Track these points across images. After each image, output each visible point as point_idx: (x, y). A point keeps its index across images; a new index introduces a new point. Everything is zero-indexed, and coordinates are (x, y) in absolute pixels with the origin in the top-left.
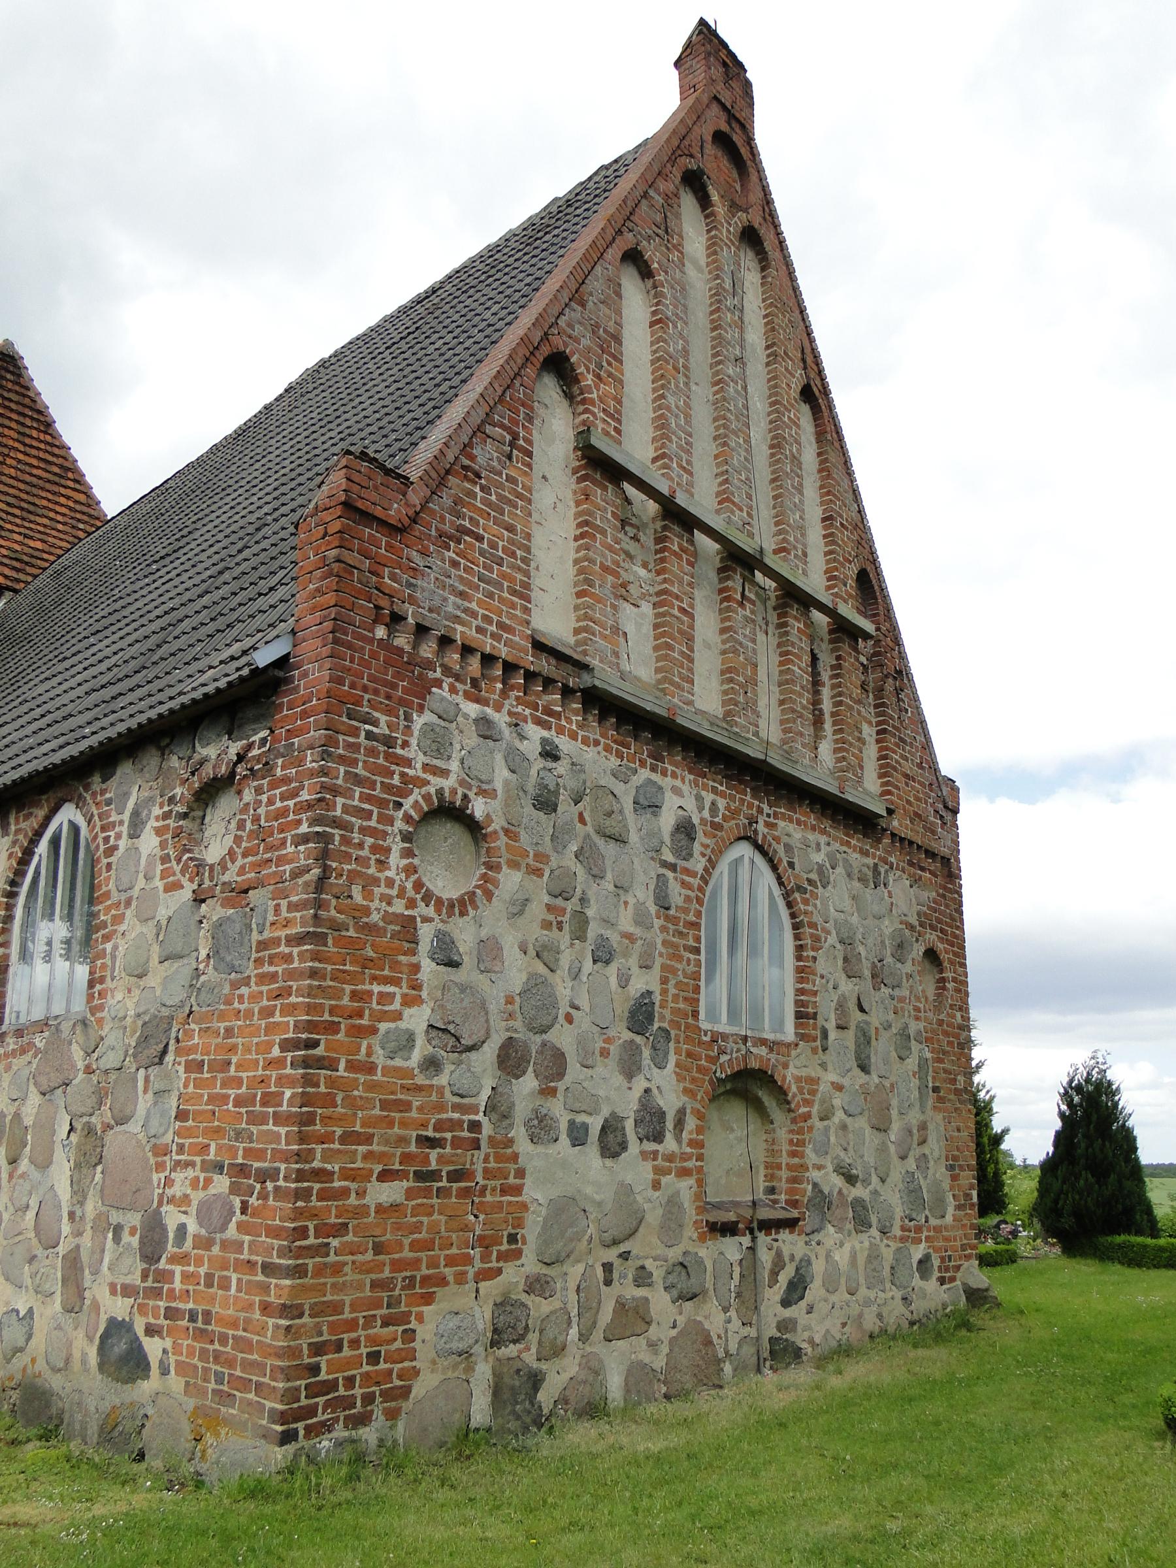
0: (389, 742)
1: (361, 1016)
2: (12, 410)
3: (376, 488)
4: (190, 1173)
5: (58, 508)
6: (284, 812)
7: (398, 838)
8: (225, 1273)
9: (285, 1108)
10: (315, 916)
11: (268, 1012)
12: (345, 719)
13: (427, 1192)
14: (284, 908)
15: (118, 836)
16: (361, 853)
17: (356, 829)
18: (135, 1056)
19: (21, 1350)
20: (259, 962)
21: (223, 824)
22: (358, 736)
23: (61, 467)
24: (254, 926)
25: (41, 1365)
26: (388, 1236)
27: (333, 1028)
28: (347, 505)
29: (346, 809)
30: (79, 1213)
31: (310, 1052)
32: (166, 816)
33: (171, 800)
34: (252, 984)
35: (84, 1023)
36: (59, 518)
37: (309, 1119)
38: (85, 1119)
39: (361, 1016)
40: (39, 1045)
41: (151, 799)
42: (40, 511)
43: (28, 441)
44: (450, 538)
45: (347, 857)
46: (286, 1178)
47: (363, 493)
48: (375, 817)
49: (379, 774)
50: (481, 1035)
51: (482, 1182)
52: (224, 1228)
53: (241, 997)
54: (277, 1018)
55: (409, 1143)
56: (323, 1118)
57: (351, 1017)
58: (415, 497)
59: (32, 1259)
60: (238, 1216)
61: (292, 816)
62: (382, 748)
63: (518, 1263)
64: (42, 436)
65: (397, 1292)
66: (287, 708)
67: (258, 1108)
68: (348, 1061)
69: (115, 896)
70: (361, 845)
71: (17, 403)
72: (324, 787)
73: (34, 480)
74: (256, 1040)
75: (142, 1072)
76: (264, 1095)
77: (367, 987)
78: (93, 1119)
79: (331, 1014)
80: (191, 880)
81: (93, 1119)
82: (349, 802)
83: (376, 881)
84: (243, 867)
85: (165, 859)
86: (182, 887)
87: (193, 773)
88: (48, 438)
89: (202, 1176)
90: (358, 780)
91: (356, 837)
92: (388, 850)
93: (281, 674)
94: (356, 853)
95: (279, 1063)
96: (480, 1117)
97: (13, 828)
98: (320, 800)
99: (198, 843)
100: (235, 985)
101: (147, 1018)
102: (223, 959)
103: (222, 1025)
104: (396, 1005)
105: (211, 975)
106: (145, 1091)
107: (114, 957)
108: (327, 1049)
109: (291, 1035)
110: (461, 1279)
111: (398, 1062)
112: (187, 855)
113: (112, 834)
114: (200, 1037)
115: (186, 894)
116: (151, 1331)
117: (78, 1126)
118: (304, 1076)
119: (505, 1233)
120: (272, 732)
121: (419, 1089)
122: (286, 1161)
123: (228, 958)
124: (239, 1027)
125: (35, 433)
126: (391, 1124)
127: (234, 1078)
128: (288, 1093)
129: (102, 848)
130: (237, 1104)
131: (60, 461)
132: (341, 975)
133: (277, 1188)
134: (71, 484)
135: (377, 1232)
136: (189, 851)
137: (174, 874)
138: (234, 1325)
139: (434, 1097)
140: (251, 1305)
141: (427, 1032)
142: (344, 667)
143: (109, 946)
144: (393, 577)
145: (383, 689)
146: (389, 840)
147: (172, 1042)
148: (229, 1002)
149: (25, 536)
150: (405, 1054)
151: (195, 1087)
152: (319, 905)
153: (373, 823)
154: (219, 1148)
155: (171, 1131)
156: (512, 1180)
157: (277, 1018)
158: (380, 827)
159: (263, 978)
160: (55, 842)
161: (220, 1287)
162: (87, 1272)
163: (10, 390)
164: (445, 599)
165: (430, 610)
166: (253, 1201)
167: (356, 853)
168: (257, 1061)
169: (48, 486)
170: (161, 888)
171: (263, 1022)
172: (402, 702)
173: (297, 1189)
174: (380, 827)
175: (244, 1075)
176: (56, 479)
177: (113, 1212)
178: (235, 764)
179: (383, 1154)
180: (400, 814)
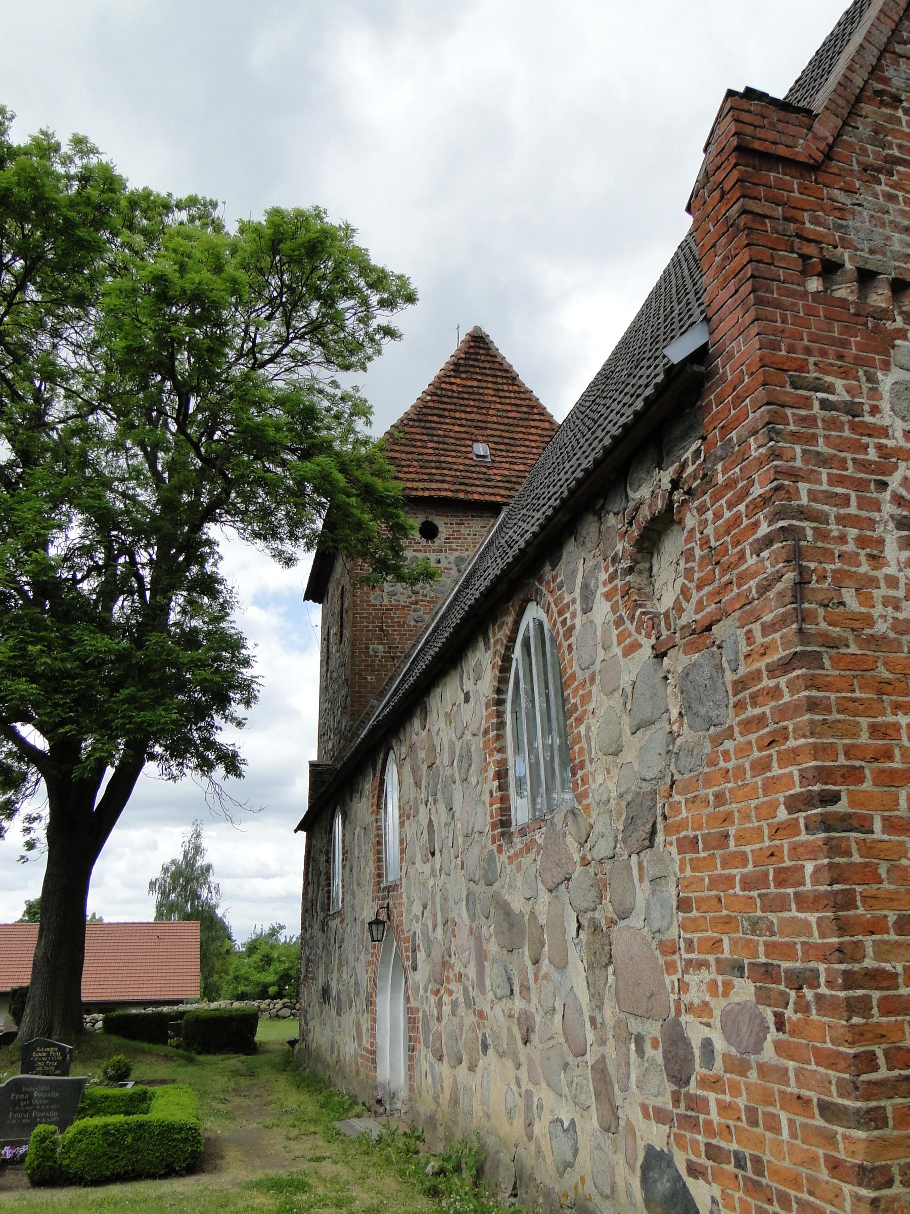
0: (853, 410)
1: (890, 757)
2: (487, 375)
3: (773, 126)
4: (706, 975)
5: (531, 437)
6: (736, 520)
7: (891, 526)
8: (770, 1109)
9: (809, 886)
10: (800, 630)
11: (762, 766)
12: (789, 389)
14: (757, 633)
15: (574, 616)
16: (844, 548)
17: (832, 519)
18: (624, 841)
19: (570, 1165)
20: (739, 706)
21: (672, 568)
22: (810, 407)
23: (528, 406)
24: (725, 665)
25: (589, 1188)
27: (853, 775)
28: (742, 150)
29: (813, 496)
30: (599, 1020)
31: (830, 809)
32: (612, 578)
33: (614, 560)
34: (737, 735)
35: (573, 812)
36: (533, 444)
37: (846, 901)
38: (589, 915)
39: (890, 757)
40: (540, 841)
41: (596, 567)
42: (518, 443)
43: (502, 394)
44: (879, 170)
45: (827, 554)
46: (830, 984)
47: (760, 133)
48: (853, 501)
49: (848, 450)
52: (758, 1048)
53: (726, 753)
54: (776, 771)
56: (864, 898)
57: (876, 760)
58: (825, 129)
59: (566, 1065)
60: (773, 1034)
61: (745, 522)
62: (845, 418)
64: (511, 388)
66: (716, 406)
67: (773, 889)
68: (884, 819)
69: (580, 676)
70: (843, 539)
71: (490, 369)
72: (778, 471)
73: (511, 421)
74: (754, 803)
75: (634, 857)
76: (778, 872)
77: (891, 719)
78: (597, 915)
79: (847, 755)
80: (648, 636)
81: (597, 915)
82: (816, 487)
83: (873, 582)
84: (700, 602)
85: (619, 622)
86: (640, 646)
87: (630, 524)
88: (515, 388)
89: (720, 979)
90: (825, 461)
91: (834, 529)
92: (881, 542)
93: (702, 369)
94: (837, 549)
95: (790, 828)
97: (492, 641)
98: (776, 489)
99: (650, 597)
100: (717, 741)
101: (629, 797)
102: (697, 714)
103: (710, 792)
105: (687, 735)
106: (641, 880)
107: (588, 739)
108: (852, 803)
109: (798, 790)
112: (640, 610)
113: (568, 615)
114: (688, 810)
115: (646, 652)
116: (694, 1171)
117: (585, 923)
118: (827, 842)
120: (704, 438)
122: (825, 959)
123: (703, 712)
124: (731, 791)
125: (506, 388)
127: (734, 855)
128: (809, 867)
129: (561, 632)
130: (747, 884)
131: (527, 402)
132: (851, 705)
133: (819, 998)
134: (537, 417)
136: (641, 606)
137: (630, 635)
138: (795, 1183)
140: (814, 1159)
142: (776, 329)
143: (582, 729)
144: (815, 221)
145: (831, 350)
146: (879, 529)
147: (659, 820)
148: (713, 763)
149: (511, 463)
151: (693, 869)
152: (803, 617)
153: (853, 510)
154: (734, 943)
155: (675, 924)
157: (776, 771)
158: (863, 514)
159: (748, 725)
160: (526, 644)
161: (768, 1128)
162: (616, 1088)
163: (483, 361)
164: (888, 238)
165: (872, 252)
166: (789, 1013)
167: (837, 549)
168: (760, 829)
169: (521, 423)
170: (620, 654)
171: (759, 780)
172: (859, 361)
173: (847, 999)
174: (863, 514)
175: (747, 849)
176: (526, 416)
177: (632, 1020)
178: (671, 493)
180: (887, 495)
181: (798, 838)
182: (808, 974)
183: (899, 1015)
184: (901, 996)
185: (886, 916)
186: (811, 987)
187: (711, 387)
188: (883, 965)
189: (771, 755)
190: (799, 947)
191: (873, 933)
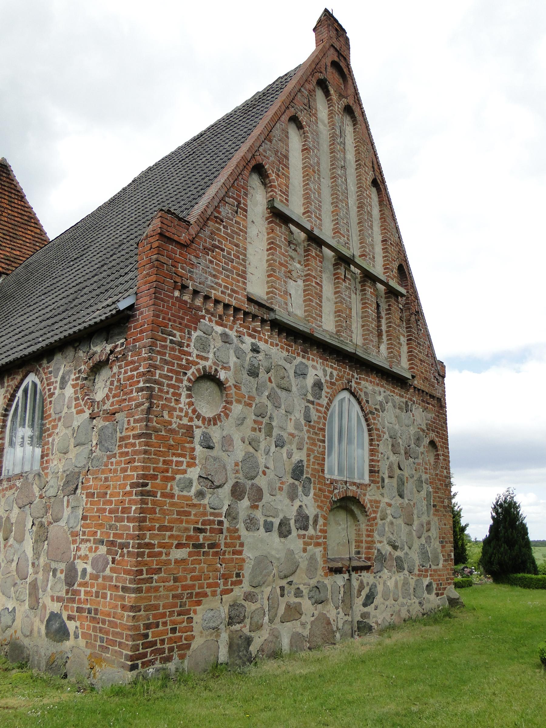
0: (181, 344)
1: (168, 472)
2: (6, 191)
3: (174, 226)
4: (88, 545)
5: (27, 236)
6: (132, 377)
7: (185, 389)
8: (105, 591)
9: (132, 514)
10: (146, 425)
11: (124, 470)
12: (160, 334)
13: (198, 554)
14: (132, 422)
15: (55, 388)
16: (167, 396)
17: (165, 385)
18: (63, 490)
19: (10, 627)
20: (120, 447)
21: (104, 383)
22: (166, 342)
23: (28, 217)
24: (118, 430)
25: (19, 634)
26: (180, 574)
27: (154, 477)
28: (161, 234)
29: (161, 376)
30: (36, 563)
31: (144, 488)
32: (77, 379)
33: (80, 371)
34: (117, 457)
35: (39, 475)
36: (28, 241)
37: (144, 520)
38: (40, 520)
39: (168, 472)
40: (18, 485)
41: (70, 371)
42: (18, 237)
43: (13, 205)
44: (209, 250)
45: (161, 398)
46: (133, 547)
47: (169, 229)
48: (174, 379)
49: (176, 359)
50: (223, 480)
51: (224, 549)
52: (104, 570)
53: (112, 463)
54: (129, 473)
55: (190, 531)
56: (150, 519)
57: (163, 472)
58: (193, 231)
59: (15, 585)
60: (110, 565)
61: (135, 379)
62: (177, 347)
63: (241, 586)
64: (19, 203)
65: (184, 600)
66: (133, 329)
67: (120, 514)
68: (161, 493)
69: (53, 416)
70: (167, 393)
71: (8, 187)
72: (150, 365)
73: (16, 223)
74: (119, 483)
75: (66, 498)
76: (123, 508)
77: (170, 458)
78: (43, 520)
79: (154, 471)
80: (89, 409)
81: (43, 520)
82: (162, 372)
83: (175, 409)
84: (113, 403)
85: (77, 399)
86: (85, 412)
87: (89, 359)
88: (22, 203)
89: (94, 546)
90: (166, 362)
91: (165, 388)
92: (180, 395)
93: (131, 313)
94: (165, 396)
95: (129, 493)
96: (223, 519)
97: (6, 384)
98: (148, 371)
99: (92, 391)
100: (109, 457)
101: (68, 473)
102: (103, 445)
103: (103, 476)
104: (184, 467)
105: (98, 453)
106: (67, 507)
107: (53, 445)
108: (152, 487)
109: (135, 481)
110: (214, 594)
111: (185, 493)
112: (87, 397)
113: (52, 387)
114: (93, 482)
115: (86, 415)
116: (70, 618)
117: (36, 523)
118: (141, 500)
119: (235, 573)
120: (126, 340)
121: (194, 505)
122: (133, 539)
123: (106, 445)
124: (111, 477)
125: (16, 201)
126: (181, 522)
127: (109, 501)
128: (134, 508)
129: (47, 394)
130: (110, 512)
131: (28, 214)
132: (158, 453)
133: (128, 552)
134: (33, 225)
135: (175, 572)
136: (88, 395)
137: (81, 406)
138: (109, 615)
139: (201, 510)
140: (117, 606)
141: (198, 479)
142: (160, 309)
143: (50, 439)
144: (182, 268)
145: (178, 320)
146: (181, 390)
147: (80, 484)
148: (106, 465)
149: (12, 249)
150: (188, 489)
151: (91, 505)
152: (148, 420)
153: (173, 382)
154: (102, 533)
155: (79, 525)
156: (238, 548)
157: (129, 473)
158: (177, 384)
159: (122, 454)
160: (26, 391)
161: (102, 598)
162: (40, 590)
163: (4, 181)
164: (207, 278)
165: (200, 283)
166: (117, 557)
167: (165, 396)
168: (119, 493)
169: (22, 226)
170: (75, 413)
171: (122, 475)
172: (187, 326)
173: (138, 552)
174: (177, 384)
175: (113, 499)
176: (26, 222)
177: (53, 563)
178: (109, 355)
179: (178, 536)
180: (186, 378)
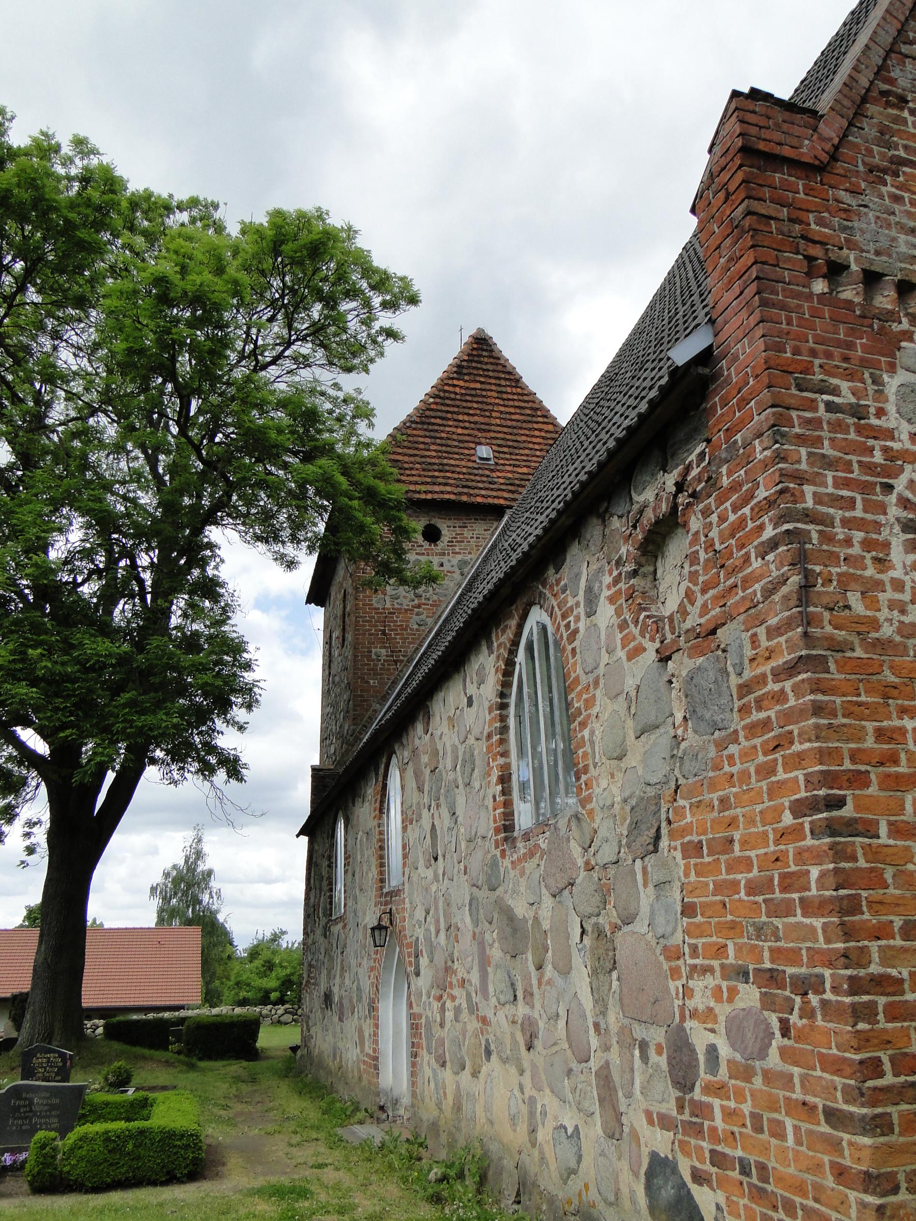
0: (858, 412)
1: (896, 762)
2: (490, 377)
3: (778, 126)
4: (710, 981)
5: (534, 440)
6: (741, 523)
7: (897, 529)
8: (775, 1116)
9: (814, 891)
10: (806, 634)
11: (767, 771)
12: (794, 391)
14: (762, 637)
15: (577, 619)
16: (850, 551)
17: (837, 522)
18: (629, 846)
19: (574, 1172)
20: (744, 710)
21: (677, 571)
22: (815, 409)
23: (531, 409)
24: (730, 669)
25: (593, 1195)
27: (859, 780)
28: (747, 151)
29: (819, 499)
30: (603, 1026)
31: (835, 813)
32: (616, 581)
33: (618, 563)
34: (742, 739)
35: (577, 817)
36: (537, 447)
37: (852, 906)
38: (593, 920)
39: (896, 762)
40: (543, 846)
41: (600, 570)
42: (522, 445)
43: (505, 396)
44: (885, 171)
45: (833, 558)
46: (835, 989)
47: (765, 134)
48: (859, 504)
49: (854, 452)
52: (763, 1054)
53: (731, 757)
54: (781, 775)
56: (870, 903)
57: (882, 764)
58: (830, 130)
59: (570, 1071)
60: (778, 1040)
61: (750, 525)
62: (851, 421)
64: (514, 390)
66: (721, 408)
67: (778, 895)
68: (890, 824)
69: (584, 680)
70: (848, 542)
71: (493, 371)
72: (783, 474)
73: (514, 424)
74: (759, 808)
75: (638, 862)
76: (783, 877)
77: (897, 723)
78: (601, 920)
79: (853, 760)
80: (652, 640)
81: (601, 920)
82: (821, 490)
83: (879, 585)
84: (705, 605)
85: (623, 626)
86: (645, 650)
87: (634, 527)
88: (519, 390)
89: (724, 985)
90: (830, 464)
91: (840, 532)
92: (887, 545)
93: (707, 371)
94: (843, 552)
95: (795, 832)
97: (495, 644)
98: (781, 492)
99: (654, 600)
100: (721, 746)
101: (633, 802)
102: (701, 718)
103: (715, 796)
105: (692, 739)
106: (645, 885)
107: (592, 743)
108: (857, 808)
109: (803, 794)
112: (644, 614)
113: (571, 618)
114: (693, 815)
115: (650, 656)
116: (699, 1177)
117: (589, 928)
118: (832, 847)
120: (708, 441)
122: (830, 965)
123: (708, 716)
124: (736, 795)
125: (509, 390)
127: (739, 860)
128: (815, 872)
129: (565, 635)
130: (752, 889)
131: (530, 405)
132: (856, 709)
133: (824, 1003)
134: (540, 419)
136: (645, 609)
137: (634, 639)
138: (801, 1189)
140: (819, 1165)
142: (781, 331)
143: (586, 733)
144: (821, 222)
145: (837, 352)
146: (885, 532)
147: (664, 824)
148: (717, 767)
149: (514, 466)
151: (698, 874)
152: (809, 620)
153: (858, 513)
154: (739, 949)
155: (680, 930)
157: (781, 775)
158: (869, 517)
159: (753, 729)
160: (530, 648)
161: (773, 1135)
162: (620, 1094)
163: (487, 363)
164: (894, 239)
165: (878, 253)
166: (794, 1018)
167: (843, 552)
168: (765, 833)
169: (524, 425)
170: (624, 658)
171: (764, 784)
172: (865, 363)
173: (853, 1005)
174: (869, 517)
175: (752, 854)
176: (530, 418)
177: (636, 1025)
178: (675, 496)
180: (893, 498)
181: (803, 843)
182: (813, 979)
183: (905, 1020)
184: (906, 1001)
185: (891, 922)
186: (816, 992)
187: (715, 389)
188: (889, 970)
189: (776, 760)
190: (804, 952)
191: (879, 938)
